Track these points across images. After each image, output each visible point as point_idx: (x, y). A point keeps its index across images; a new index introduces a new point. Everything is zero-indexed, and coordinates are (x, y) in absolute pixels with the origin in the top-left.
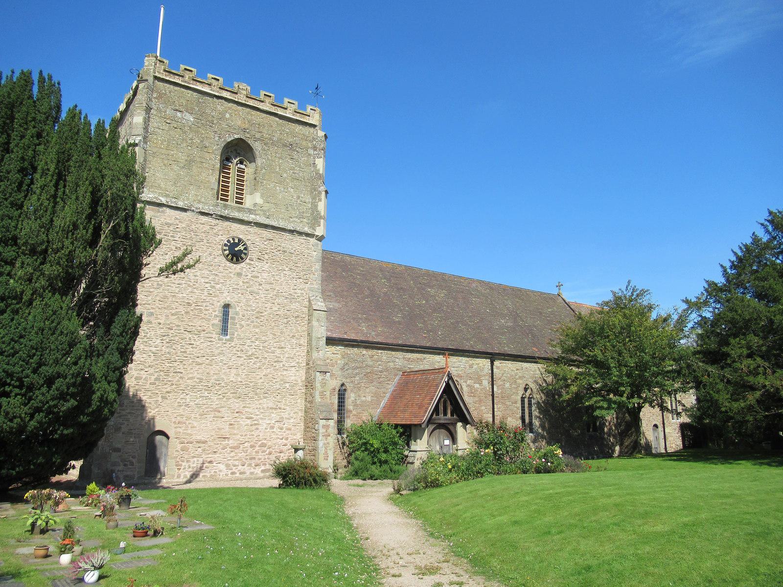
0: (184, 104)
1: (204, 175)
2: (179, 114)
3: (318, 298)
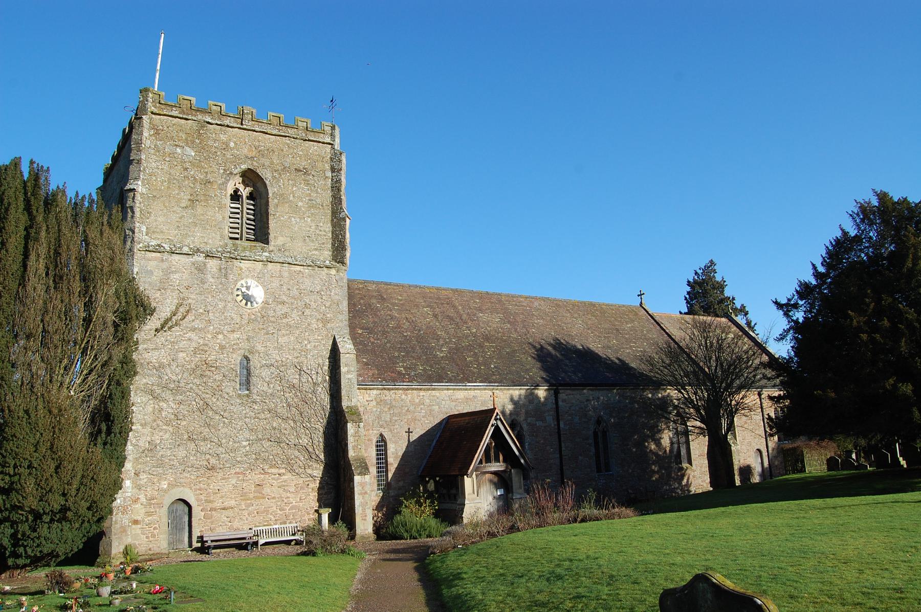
0: (184, 138)
1: (209, 213)
2: (179, 150)
3: (346, 339)
